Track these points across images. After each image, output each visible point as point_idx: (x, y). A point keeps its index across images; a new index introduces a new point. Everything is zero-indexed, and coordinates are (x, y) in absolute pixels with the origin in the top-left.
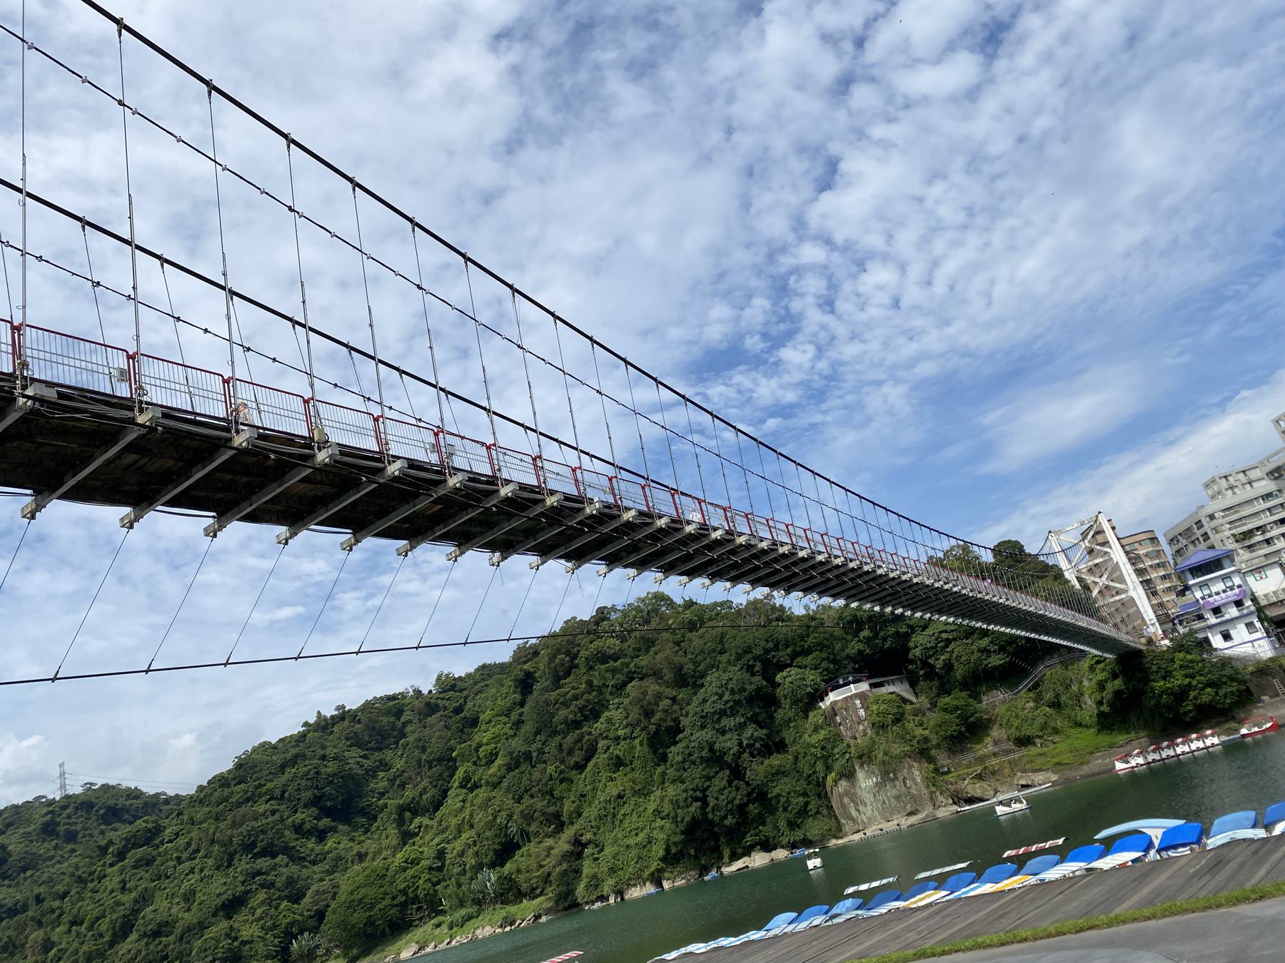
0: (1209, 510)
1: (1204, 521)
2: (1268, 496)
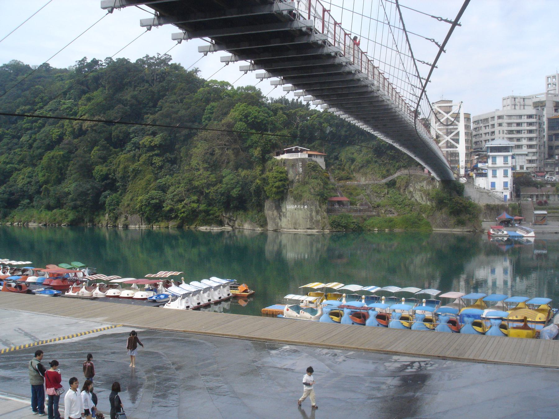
0: (500, 114)
1: (496, 118)
2: (530, 116)
